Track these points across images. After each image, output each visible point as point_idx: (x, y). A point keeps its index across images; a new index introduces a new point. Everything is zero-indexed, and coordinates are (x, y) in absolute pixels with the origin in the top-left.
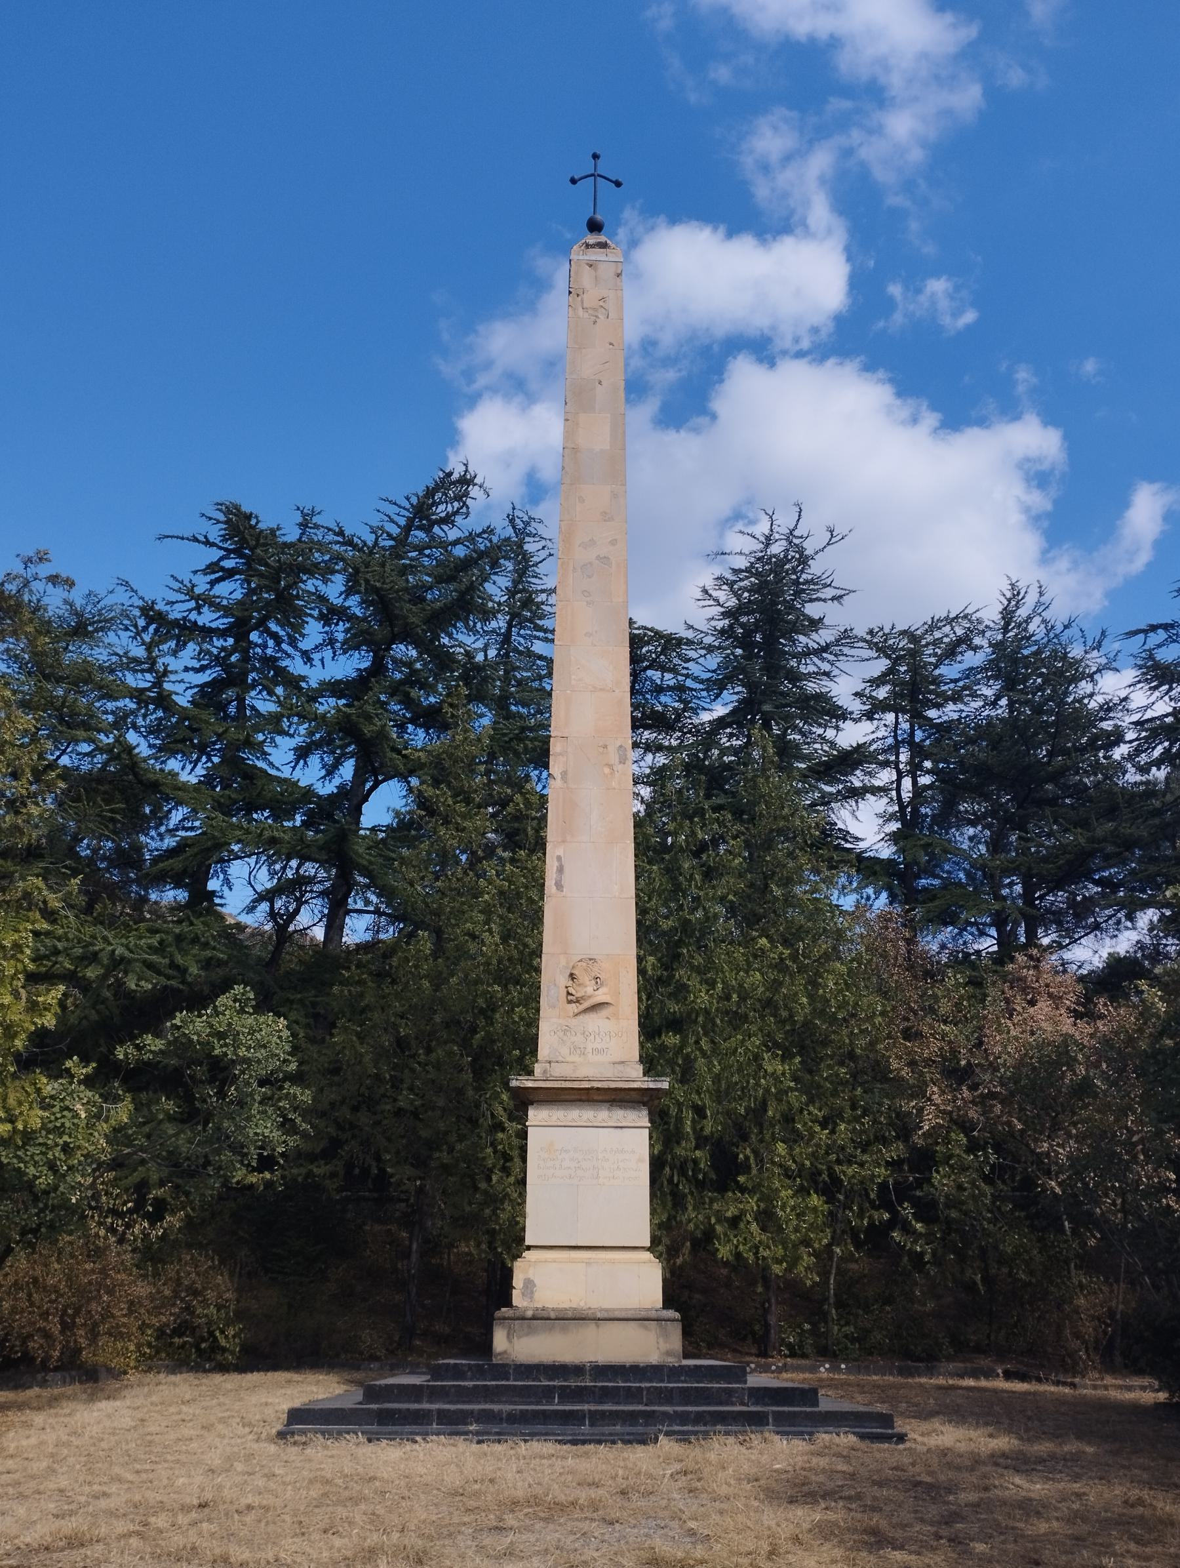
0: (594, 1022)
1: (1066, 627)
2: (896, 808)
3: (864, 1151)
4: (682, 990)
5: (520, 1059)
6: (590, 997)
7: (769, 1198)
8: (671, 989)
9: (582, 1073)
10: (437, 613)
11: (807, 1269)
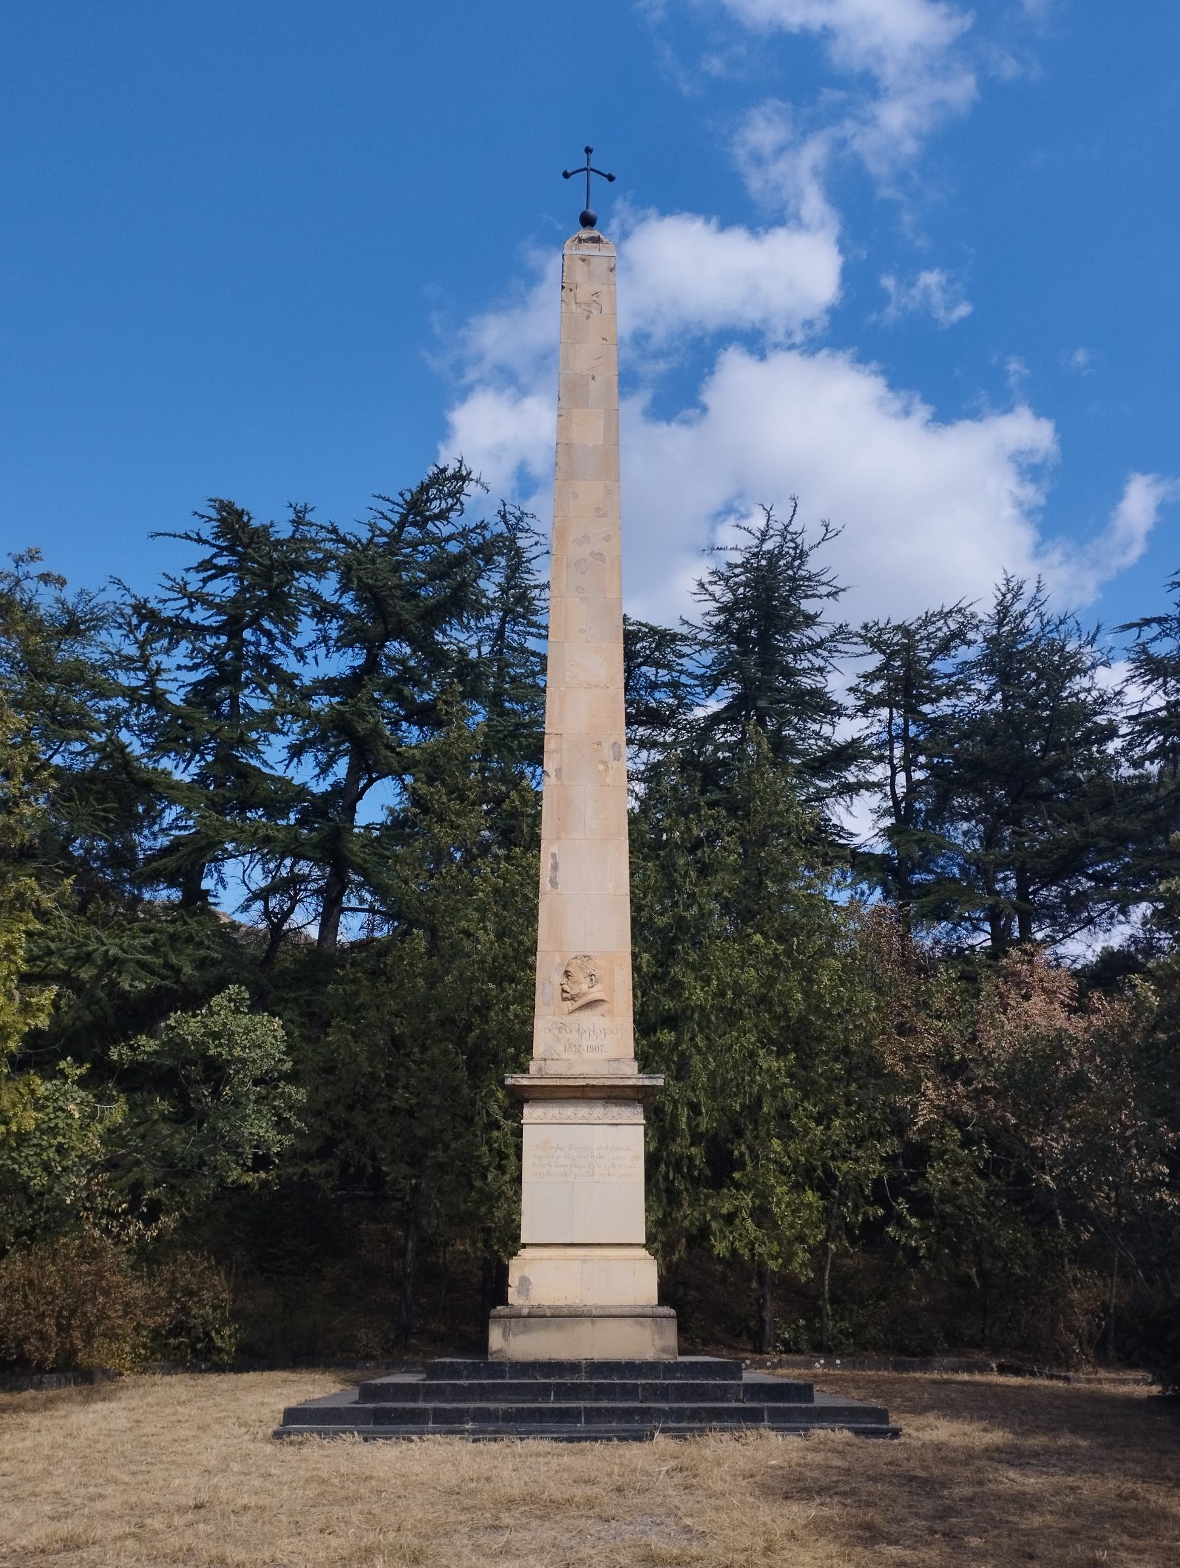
0: (589, 1019)
1: (1062, 622)
2: (891, 803)
3: (858, 1147)
4: (676, 987)
5: (515, 1058)
6: (584, 994)
7: (764, 1195)
8: (666, 986)
9: (576, 1070)
10: (432, 609)
11: (803, 1265)
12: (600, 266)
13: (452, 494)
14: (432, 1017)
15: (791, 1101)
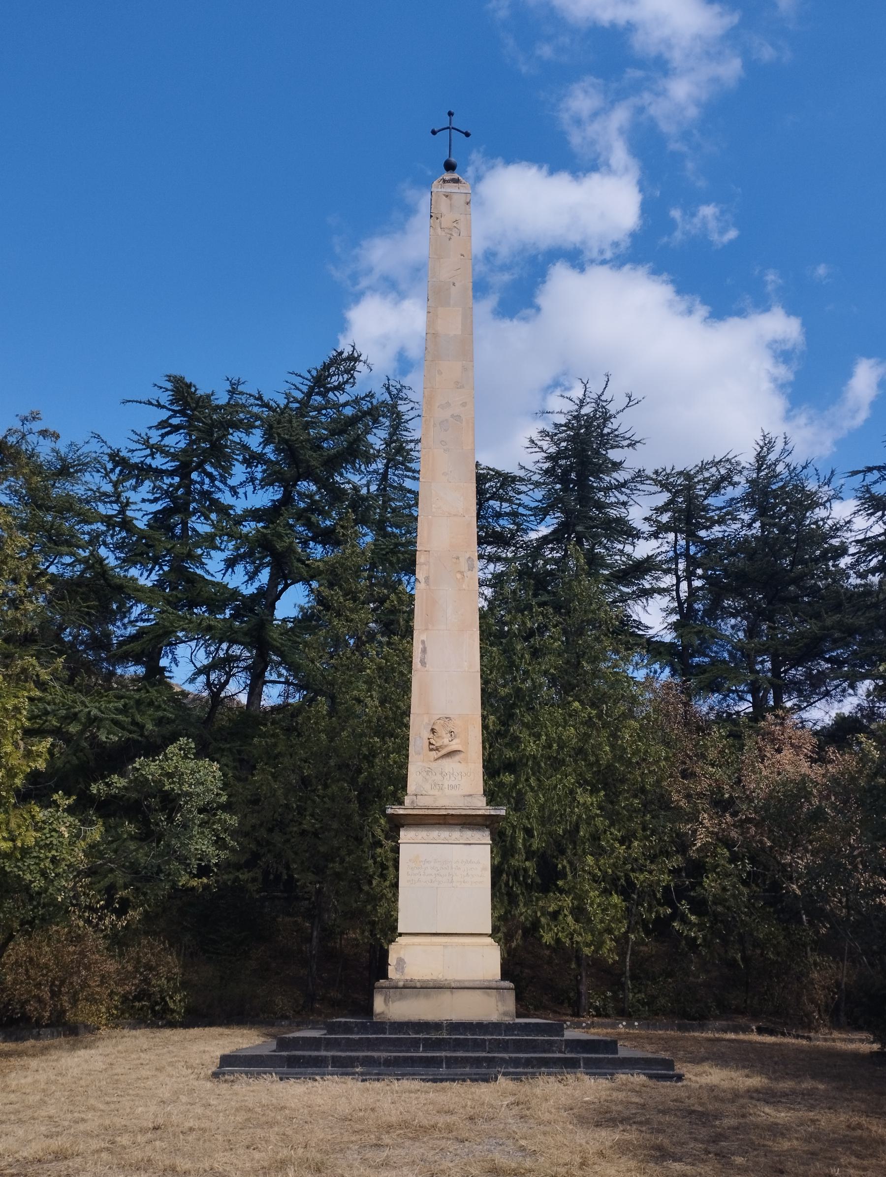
0: (449, 765)
1: (804, 468)
2: (676, 604)
3: (652, 862)
5: (394, 793)
6: (446, 746)
7: (581, 897)
9: (440, 803)
10: (331, 458)
11: (610, 950)
12: (459, 200)
13: (347, 371)
14: (332, 763)
15: (601, 827)
